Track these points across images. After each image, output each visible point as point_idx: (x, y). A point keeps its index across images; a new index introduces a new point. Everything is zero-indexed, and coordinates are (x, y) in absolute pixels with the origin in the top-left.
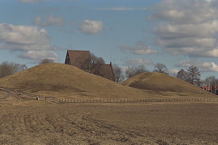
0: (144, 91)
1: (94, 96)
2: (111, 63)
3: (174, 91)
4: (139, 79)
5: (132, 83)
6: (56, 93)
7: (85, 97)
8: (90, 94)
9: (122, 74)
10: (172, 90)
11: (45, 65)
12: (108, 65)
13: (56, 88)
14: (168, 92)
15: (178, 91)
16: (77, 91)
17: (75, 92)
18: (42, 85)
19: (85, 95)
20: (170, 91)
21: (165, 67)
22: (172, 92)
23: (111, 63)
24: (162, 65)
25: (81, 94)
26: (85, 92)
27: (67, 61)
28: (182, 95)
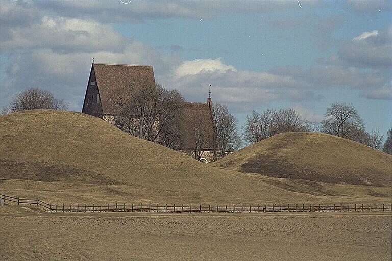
0: (280, 184)
1: (139, 195)
2: (209, 99)
3: (359, 183)
4: (269, 149)
5: (250, 160)
6: (49, 185)
7: (117, 196)
8: (130, 189)
9: (235, 133)
10: (354, 180)
11: (24, 115)
12: (200, 105)
13: (48, 173)
14: (342, 186)
15: (370, 184)
16: (101, 180)
17: (94, 183)
18: (16, 166)
19: (118, 193)
20: (347, 182)
21: (354, 113)
22: (353, 186)
23: (209, 99)
24: (347, 109)
25: (109, 189)
26: (118, 183)
27: (92, 105)
28: (376, 195)
